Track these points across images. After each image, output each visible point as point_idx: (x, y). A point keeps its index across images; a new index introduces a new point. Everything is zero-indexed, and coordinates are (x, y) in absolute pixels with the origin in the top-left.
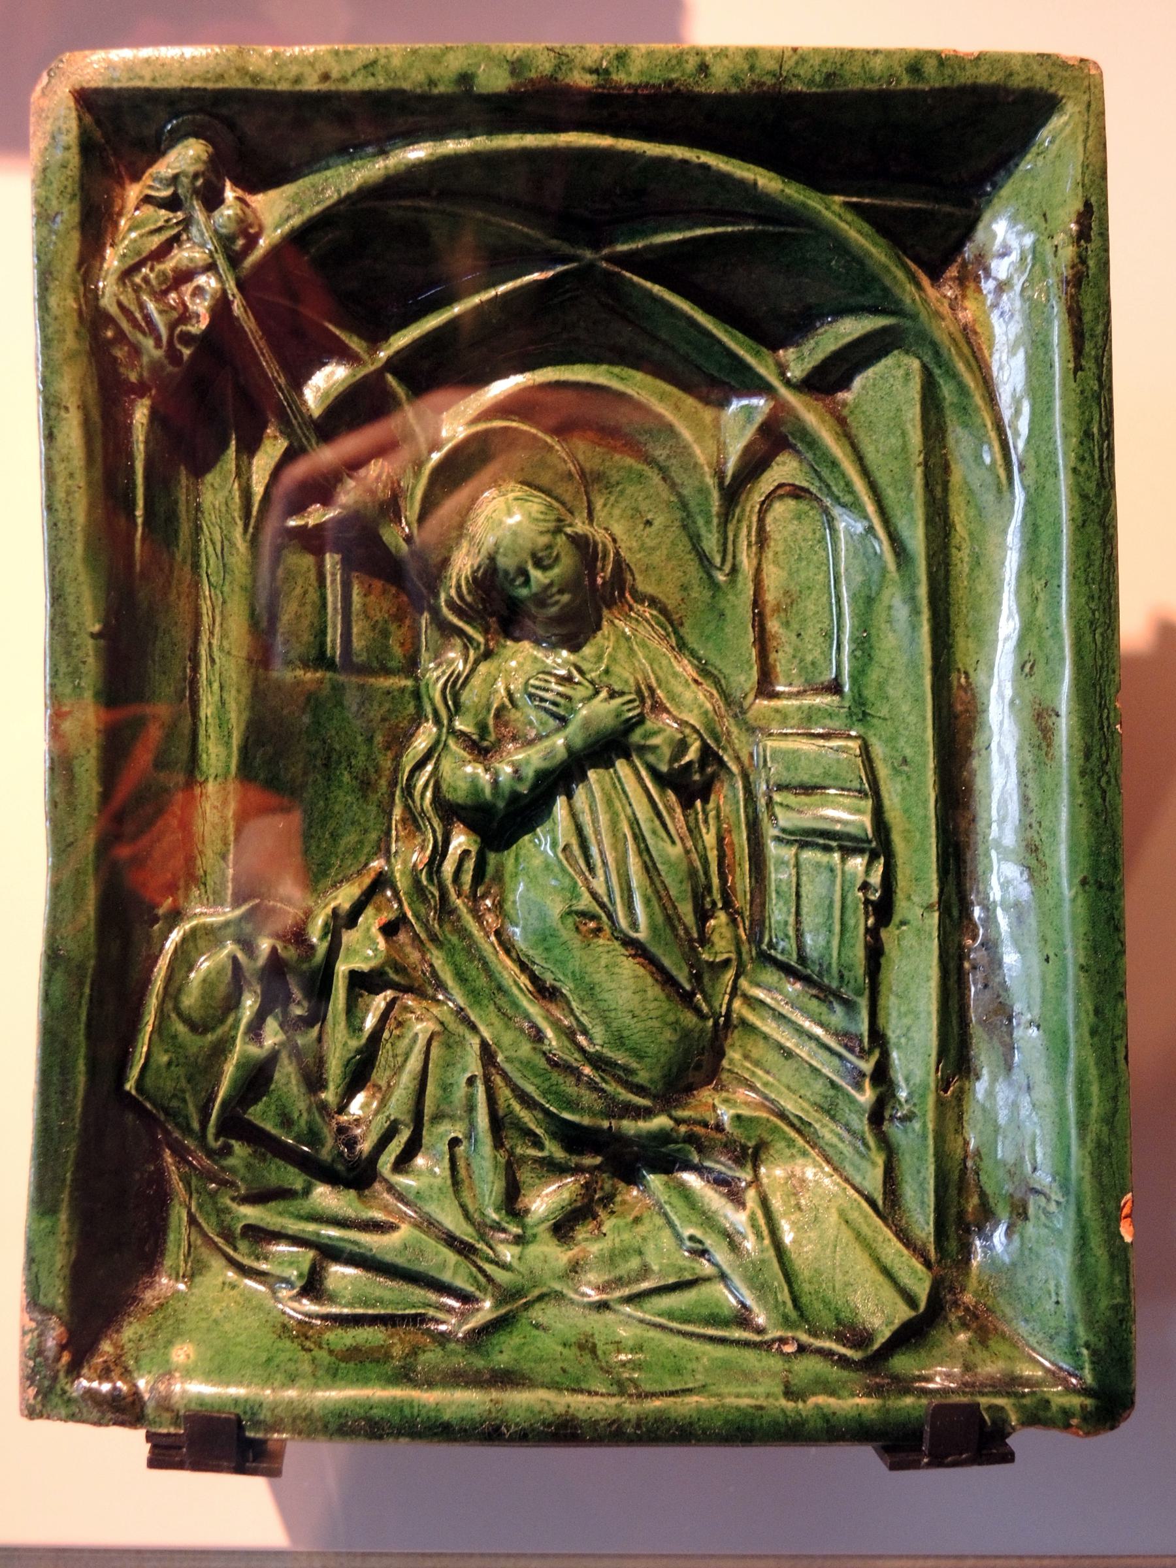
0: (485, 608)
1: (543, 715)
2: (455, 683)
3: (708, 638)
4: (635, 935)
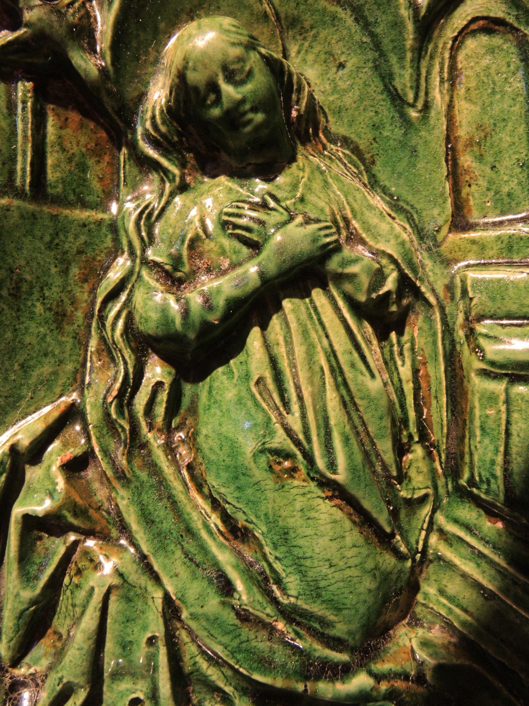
0: (181, 141)
1: (238, 245)
2: (150, 215)
3: (400, 174)
4: (333, 477)
